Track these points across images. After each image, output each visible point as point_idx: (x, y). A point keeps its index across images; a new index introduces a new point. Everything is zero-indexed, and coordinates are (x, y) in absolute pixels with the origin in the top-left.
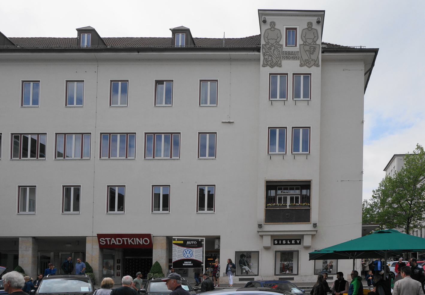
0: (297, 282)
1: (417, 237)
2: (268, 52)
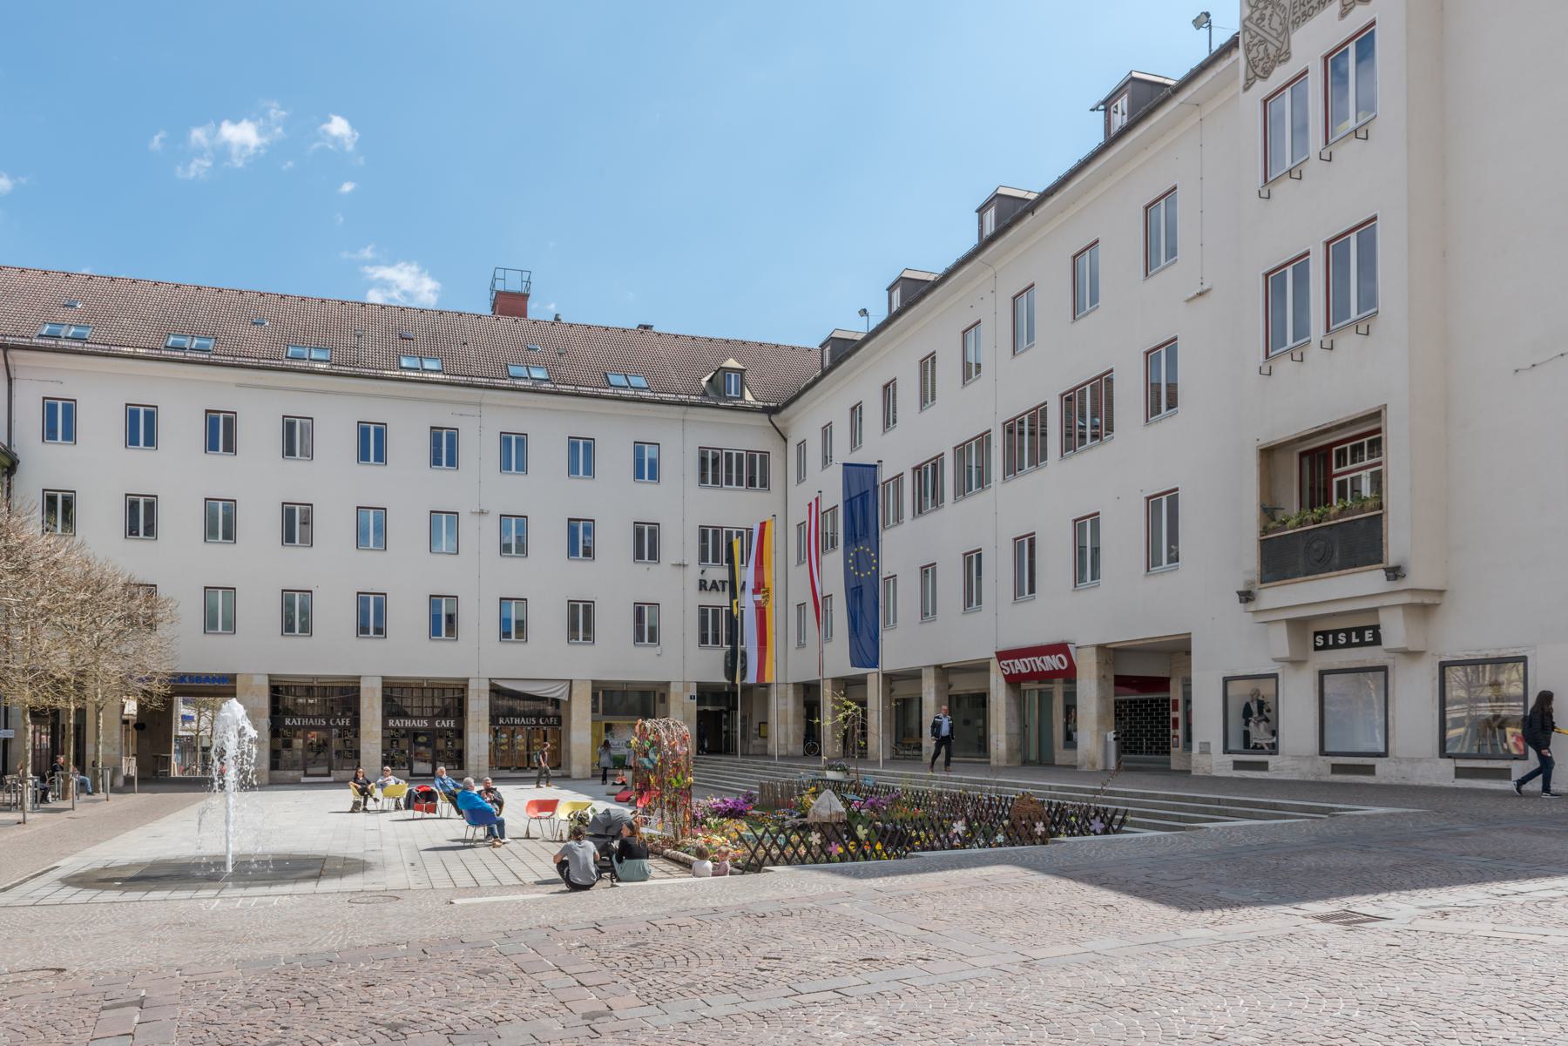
0: (1384, 782)
1: (298, 726)
2: (1258, 34)
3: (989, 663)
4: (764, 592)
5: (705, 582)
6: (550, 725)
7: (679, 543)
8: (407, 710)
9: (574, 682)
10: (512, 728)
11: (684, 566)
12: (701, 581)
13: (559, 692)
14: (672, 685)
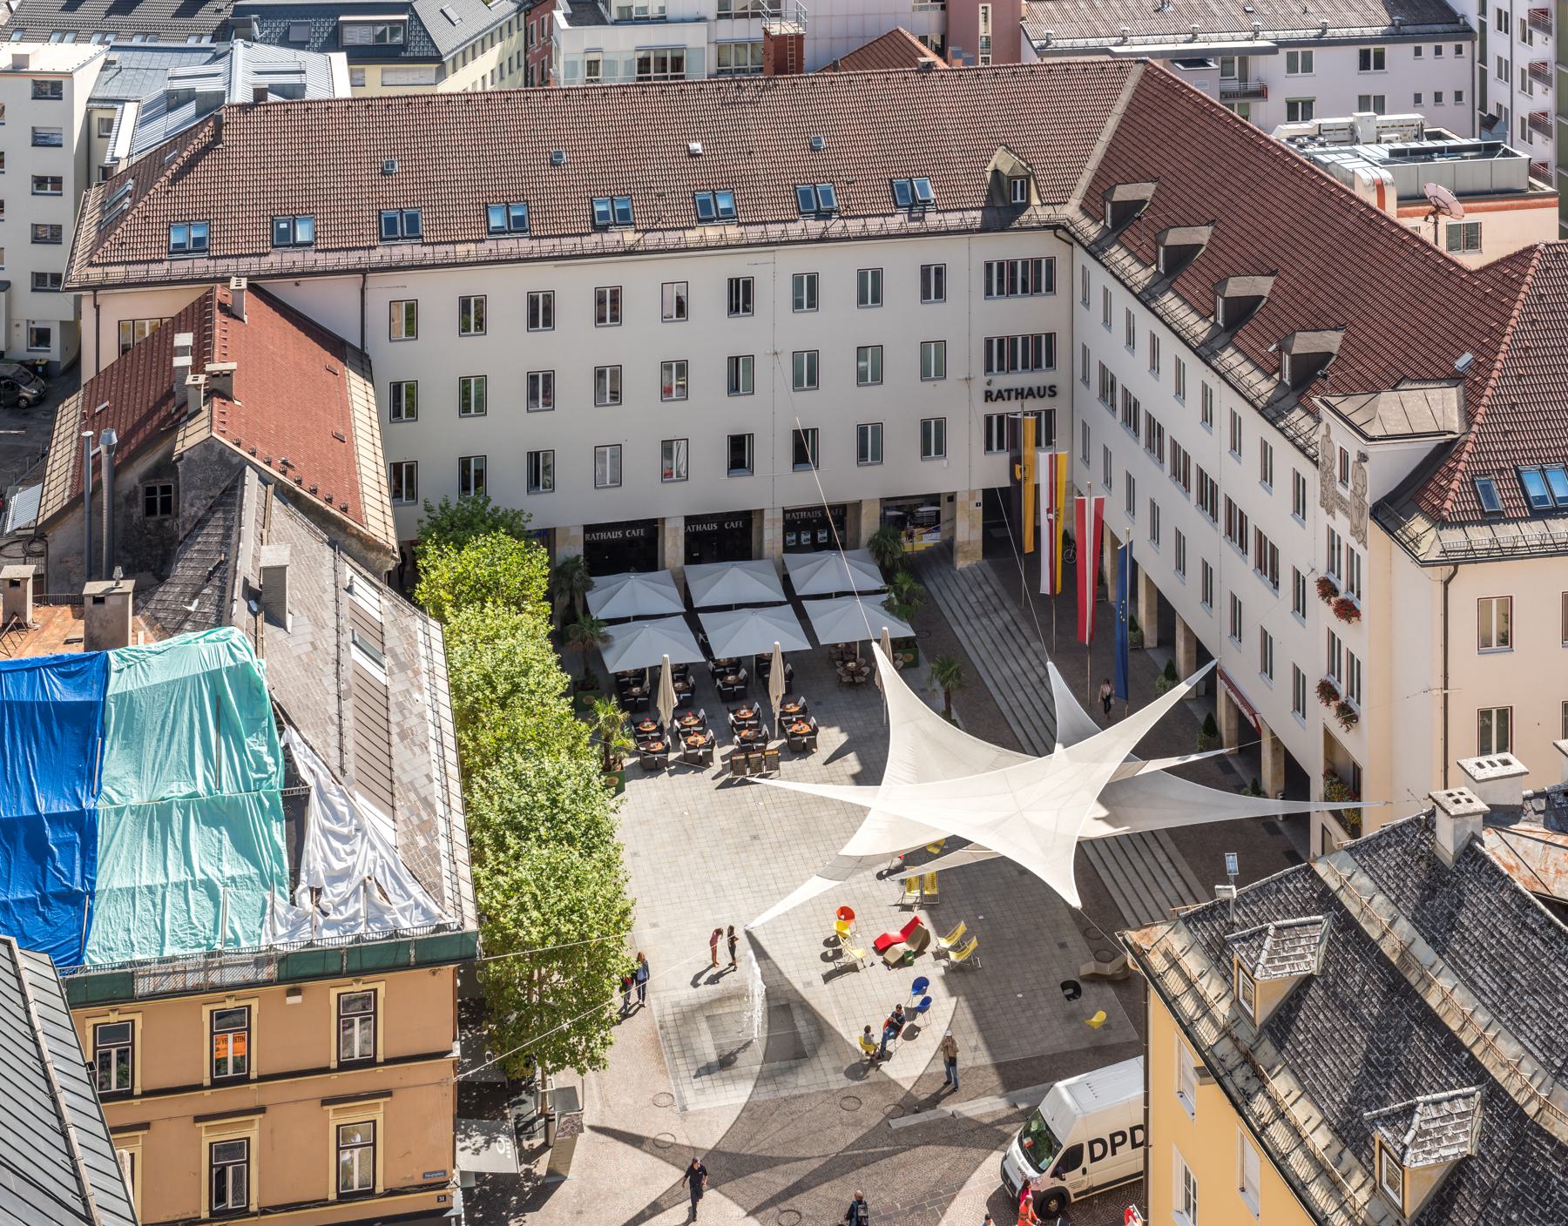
5: (991, 393)
7: (965, 358)
12: (987, 392)
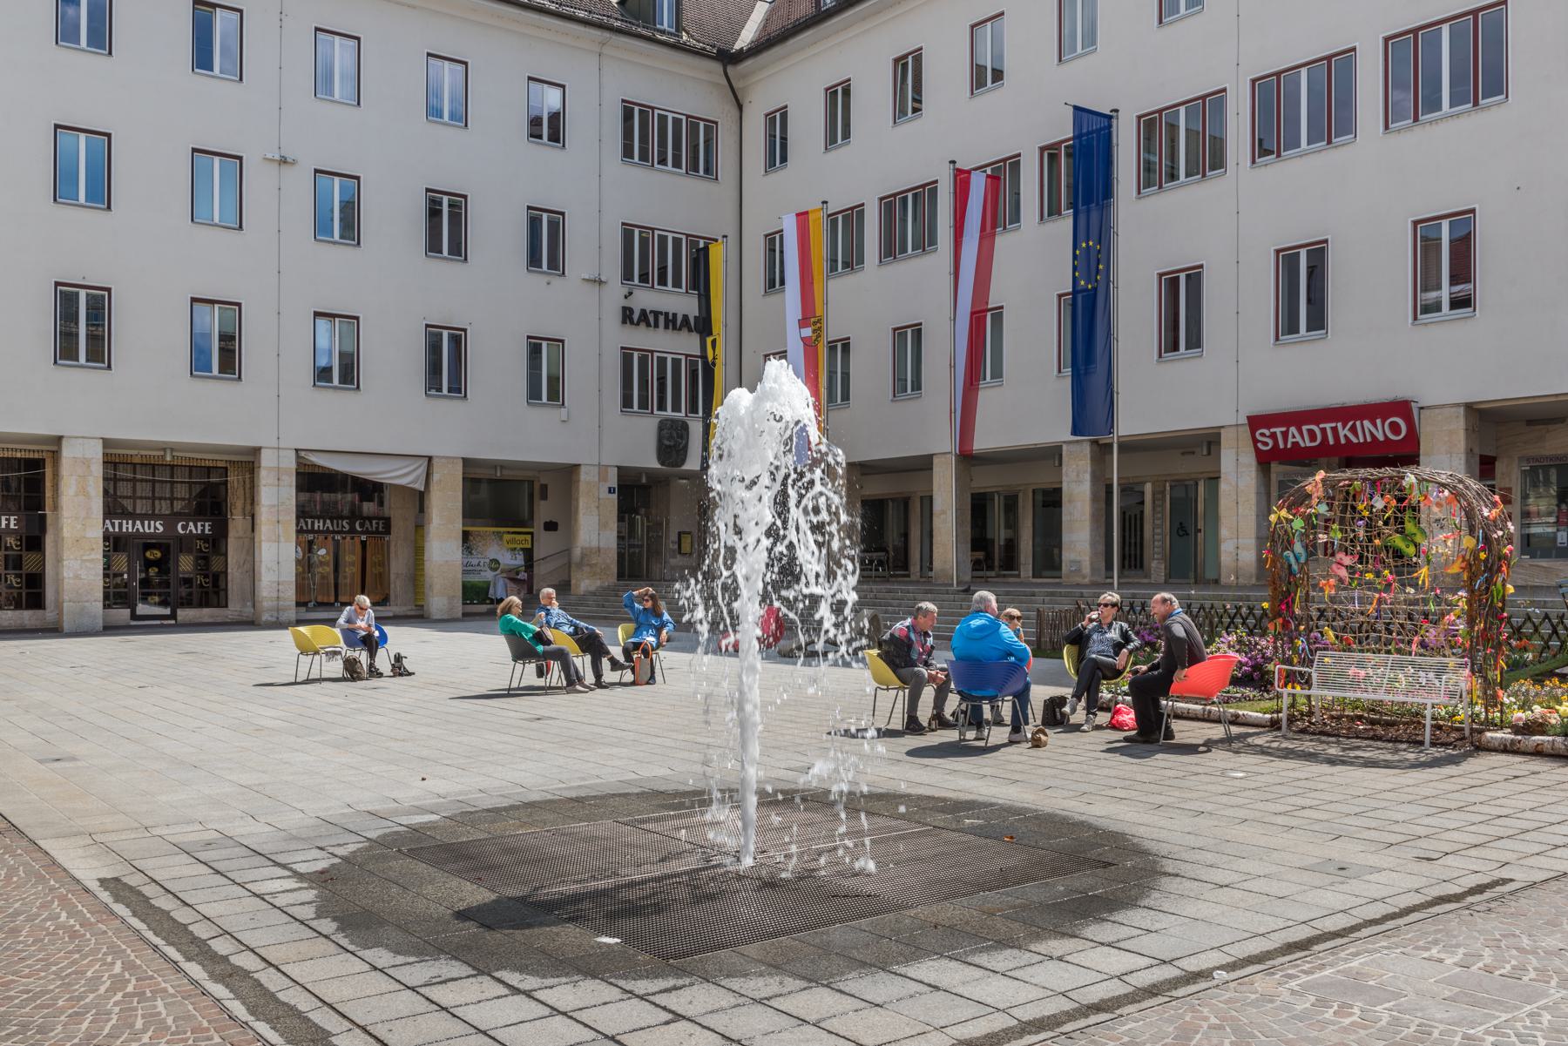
3: (1219, 434)
4: (815, 323)
6: (373, 533)
8: (125, 502)
9: (435, 461)
10: (311, 537)
11: (601, 282)
12: (625, 309)
13: (404, 475)
14: (583, 469)
